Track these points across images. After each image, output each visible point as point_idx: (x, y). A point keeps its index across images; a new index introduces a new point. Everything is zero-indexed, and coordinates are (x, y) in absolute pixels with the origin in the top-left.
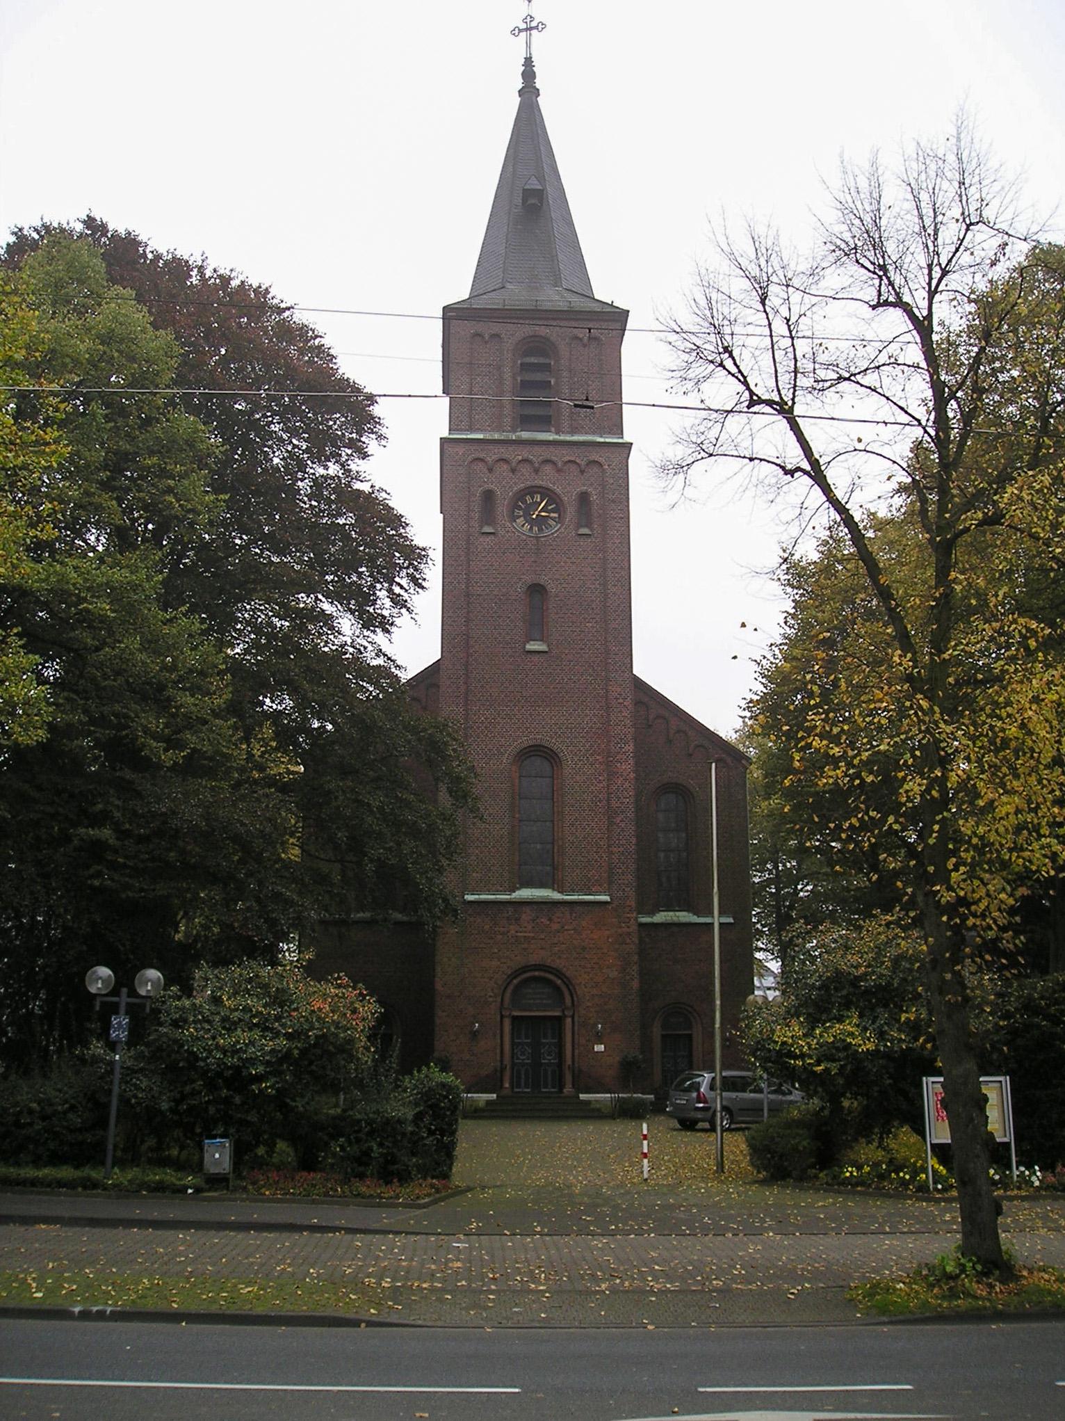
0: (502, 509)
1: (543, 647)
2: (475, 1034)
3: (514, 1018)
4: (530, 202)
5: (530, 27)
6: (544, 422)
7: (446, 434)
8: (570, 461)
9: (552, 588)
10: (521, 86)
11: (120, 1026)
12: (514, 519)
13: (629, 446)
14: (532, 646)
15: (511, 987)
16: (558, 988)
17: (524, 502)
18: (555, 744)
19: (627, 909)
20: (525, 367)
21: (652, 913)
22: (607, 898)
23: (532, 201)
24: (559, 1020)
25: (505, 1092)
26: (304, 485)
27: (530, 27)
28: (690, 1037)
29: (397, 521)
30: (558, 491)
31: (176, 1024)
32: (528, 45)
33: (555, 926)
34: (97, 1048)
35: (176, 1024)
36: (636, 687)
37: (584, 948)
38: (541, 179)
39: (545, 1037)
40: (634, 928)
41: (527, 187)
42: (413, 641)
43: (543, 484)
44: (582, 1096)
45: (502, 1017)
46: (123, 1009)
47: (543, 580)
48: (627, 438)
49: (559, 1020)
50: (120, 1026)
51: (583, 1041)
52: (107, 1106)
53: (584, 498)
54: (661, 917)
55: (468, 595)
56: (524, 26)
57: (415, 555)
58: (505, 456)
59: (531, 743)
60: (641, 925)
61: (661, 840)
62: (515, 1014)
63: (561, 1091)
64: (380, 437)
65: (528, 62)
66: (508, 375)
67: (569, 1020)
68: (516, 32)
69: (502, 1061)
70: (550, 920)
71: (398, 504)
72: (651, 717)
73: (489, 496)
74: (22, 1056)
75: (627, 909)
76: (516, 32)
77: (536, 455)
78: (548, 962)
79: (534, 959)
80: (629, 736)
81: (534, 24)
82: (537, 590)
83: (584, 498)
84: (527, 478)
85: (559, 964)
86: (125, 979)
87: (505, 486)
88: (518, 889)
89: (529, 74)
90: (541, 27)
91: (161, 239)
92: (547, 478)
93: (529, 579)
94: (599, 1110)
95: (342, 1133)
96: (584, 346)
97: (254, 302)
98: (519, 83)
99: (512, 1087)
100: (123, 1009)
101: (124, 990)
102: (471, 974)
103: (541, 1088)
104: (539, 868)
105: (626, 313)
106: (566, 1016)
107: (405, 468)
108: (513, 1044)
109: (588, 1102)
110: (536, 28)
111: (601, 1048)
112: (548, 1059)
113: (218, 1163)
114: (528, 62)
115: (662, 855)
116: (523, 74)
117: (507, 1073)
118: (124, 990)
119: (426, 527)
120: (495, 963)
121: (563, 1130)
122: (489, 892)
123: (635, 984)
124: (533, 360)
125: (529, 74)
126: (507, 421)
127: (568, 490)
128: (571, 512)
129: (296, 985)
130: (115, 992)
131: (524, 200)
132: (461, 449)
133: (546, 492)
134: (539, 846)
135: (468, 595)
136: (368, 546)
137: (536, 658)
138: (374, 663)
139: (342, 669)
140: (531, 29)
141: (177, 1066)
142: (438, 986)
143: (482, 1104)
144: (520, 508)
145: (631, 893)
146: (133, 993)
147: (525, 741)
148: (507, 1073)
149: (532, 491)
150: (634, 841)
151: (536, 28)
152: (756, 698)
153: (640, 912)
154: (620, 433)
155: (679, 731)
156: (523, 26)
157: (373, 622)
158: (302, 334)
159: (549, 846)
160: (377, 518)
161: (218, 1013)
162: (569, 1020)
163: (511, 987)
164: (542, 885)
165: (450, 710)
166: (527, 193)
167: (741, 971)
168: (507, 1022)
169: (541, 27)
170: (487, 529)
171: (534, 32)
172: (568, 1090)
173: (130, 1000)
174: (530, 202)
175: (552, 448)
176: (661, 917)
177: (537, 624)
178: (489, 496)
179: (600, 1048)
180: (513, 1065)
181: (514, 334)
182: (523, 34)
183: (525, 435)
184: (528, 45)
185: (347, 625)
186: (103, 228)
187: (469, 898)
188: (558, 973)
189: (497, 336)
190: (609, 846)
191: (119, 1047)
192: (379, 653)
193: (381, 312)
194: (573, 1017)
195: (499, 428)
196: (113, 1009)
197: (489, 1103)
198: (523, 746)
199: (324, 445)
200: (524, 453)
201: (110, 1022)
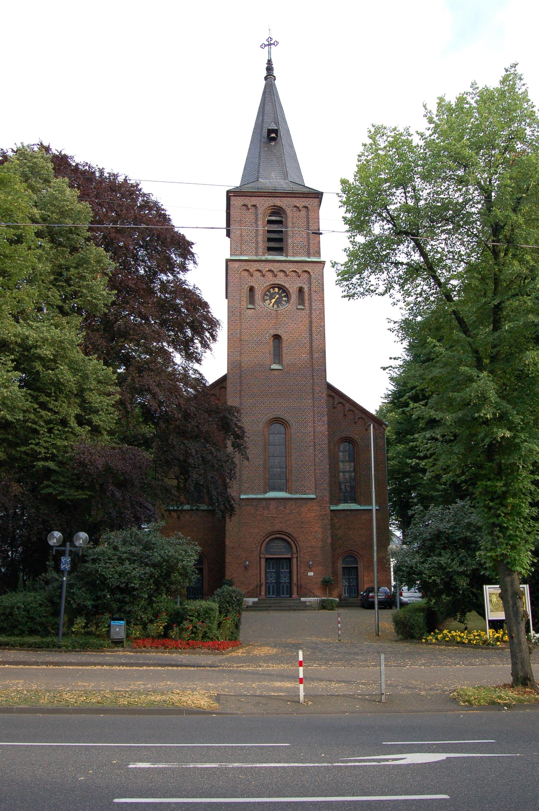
0: (258, 295)
1: (279, 367)
2: (246, 567)
3: (267, 559)
4: (270, 135)
5: (270, 44)
6: (280, 250)
7: (229, 257)
8: (293, 271)
9: (284, 337)
10: (265, 75)
11: (66, 563)
12: (264, 300)
13: (323, 263)
14: (274, 366)
15: (265, 543)
16: (288, 543)
17: (269, 292)
18: (287, 417)
19: (325, 502)
20: (269, 222)
21: (337, 504)
22: (314, 496)
23: (273, 135)
24: (290, 560)
25: (261, 597)
26: (157, 286)
27: (270, 44)
28: (357, 567)
29: (205, 305)
30: (287, 286)
31: (94, 561)
32: (269, 53)
33: (288, 511)
34: (52, 574)
35: (94, 561)
36: (328, 387)
37: (302, 523)
38: (277, 123)
39: (283, 569)
40: (328, 512)
41: (270, 128)
42: (213, 364)
43: (280, 283)
44: (303, 599)
45: (260, 558)
46: (67, 553)
47: (279, 333)
48: (322, 259)
49: (290, 560)
50: (66, 563)
51: (302, 571)
52: (59, 604)
53: (301, 290)
54: (342, 506)
55: (241, 340)
56: (267, 43)
57: (213, 324)
58: (260, 268)
59: (274, 417)
60: (331, 510)
61: (341, 467)
62: (268, 556)
63: (291, 596)
64: (195, 263)
65: (269, 62)
66: (260, 228)
67: (295, 560)
68: (263, 46)
69: (260, 581)
70: (285, 508)
71: (205, 297)
72: (336, 403)
73: (252, 289)
74: (8, 583)
75: (325, 502)
76: (263, 46)
77: (276, 267)
78: (284, 529)
79: (276, 528)
80: (325, 413)
81: (272, 42)
82: (277, 337)
83: (301, 290)
84: (270, 280)
85: (289, 530)
86: (68, 537)
87: (260, 284)
88: (268, 492)
89: (270, 69)
90: (276, 43)
91: (80, 156)
92: (281, 280)
93: (273, 332)
94: (311, 606)
95: (185, 607)
96: (300, 211)
97: (128, 191)
98: (265, 73)
99: (266, 595)
100: (67, 553)
101: (68, 544)
102: (243, 538)
103: (281, 589)
104: (279, 481)
105: (322, 194)
106: (293, 557)
107: (207, 276)
108: (266, 572)
109: (305, 602)
110: (274, 44)
111: (311, 574)
112: (284, 580)
113: (117, 633)
114: (269, 62)
115: (341, 474)
116: (266, 78)
117: (263, 588)
118: (68, 544)
119: (219, 308)
120: (256, 530)
121: (293, 615)
122: (253, 493)
123: (329, 541)
124: (273, 218)
125: (270, 69)
126: (260, 250)
127: (292, 287)
128: (294, 297)
129: (158, 539)
130: (63, 544)
131: (269, 135)
132: (236, 265)
133: (281, 288)
134: (278, 470)
135: (241, 340)
136: (189, 319)
137: (276, 372)
138: (193, 376)
139: (174, 380)
140: (271, 44)
141: (95, 584)
142: (227, 543)
143: (250, 604)
144: (267, 295)
145: (327, 494)
146: (73, 545)
147: (271, 416)
148: (263, 588)
149: (273, 286)
150: (328, 466)
151: (274, 44)
152: (390, 393)
153: (332, 503)
154: (318, 253)
155: (350, 410)
156: (267, 43)
157: (192, 356)
158: (156, 207)
159: (284, 458)
160: (196, 303)
161: (116, 555)
162: (295, 560)
163: (265, 543)
164: (281, 490)
165: (232, 401)
166: (270, 131)
167: (385, 537)
168: (263, 561)
169: (276, 43)
170: (250, 306)
171: (272, 46)
172: (295, 596)
173: (71, 549)
174: (270, 135)
175: (284, 264)
176: (342, 506)
177: (278, 356)
178: (252, 289)
179: (311, 574)
180: (266, 583)
181: (264, 204)
182: (267, 48)
183: (270, 257)
184: (269, 53)
185: (178, 358)
186: (48, 149)
187: (242, 497)
188: (289, 535)
189: (254, 206)
190: (315, 470)
191: (66, 573)
192: (196, 371)
193: (194, 194)
194: (297, 558)
195: (257, 255)
196: (63, 553)
197: (254, 603)
198: (270, 418)
199: (169, 266)
200: (270, 266)
201: (60, 560)
